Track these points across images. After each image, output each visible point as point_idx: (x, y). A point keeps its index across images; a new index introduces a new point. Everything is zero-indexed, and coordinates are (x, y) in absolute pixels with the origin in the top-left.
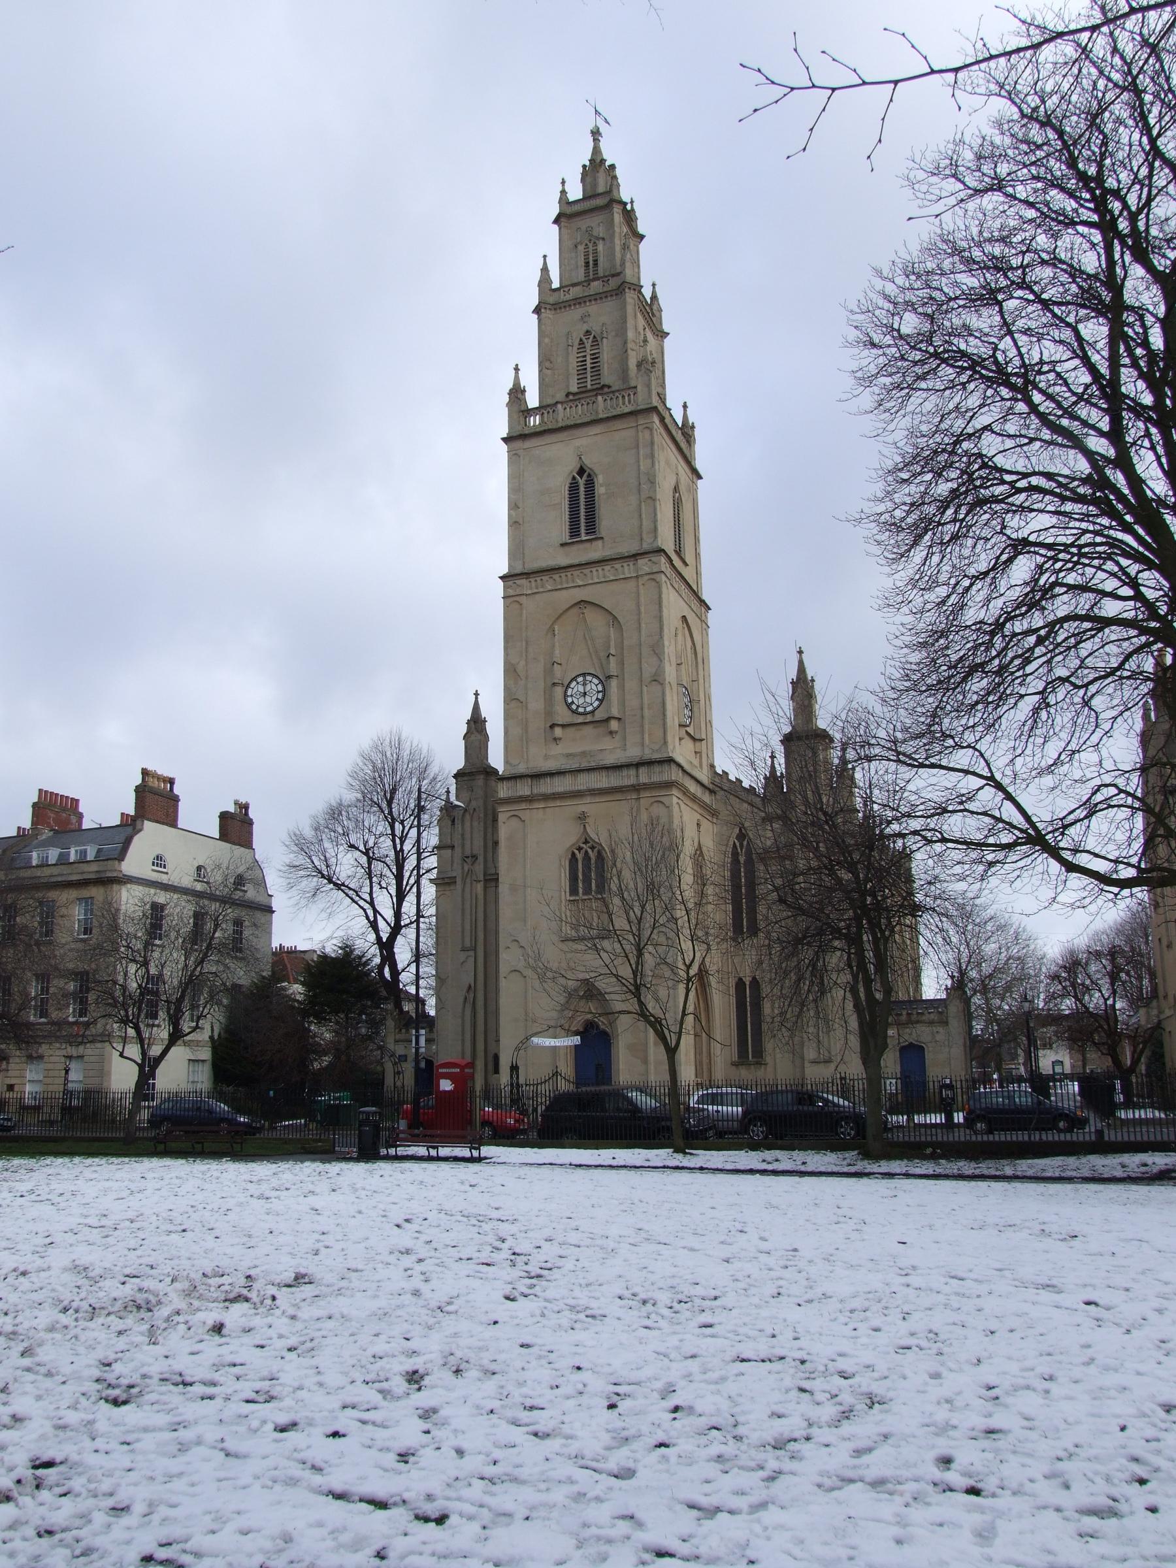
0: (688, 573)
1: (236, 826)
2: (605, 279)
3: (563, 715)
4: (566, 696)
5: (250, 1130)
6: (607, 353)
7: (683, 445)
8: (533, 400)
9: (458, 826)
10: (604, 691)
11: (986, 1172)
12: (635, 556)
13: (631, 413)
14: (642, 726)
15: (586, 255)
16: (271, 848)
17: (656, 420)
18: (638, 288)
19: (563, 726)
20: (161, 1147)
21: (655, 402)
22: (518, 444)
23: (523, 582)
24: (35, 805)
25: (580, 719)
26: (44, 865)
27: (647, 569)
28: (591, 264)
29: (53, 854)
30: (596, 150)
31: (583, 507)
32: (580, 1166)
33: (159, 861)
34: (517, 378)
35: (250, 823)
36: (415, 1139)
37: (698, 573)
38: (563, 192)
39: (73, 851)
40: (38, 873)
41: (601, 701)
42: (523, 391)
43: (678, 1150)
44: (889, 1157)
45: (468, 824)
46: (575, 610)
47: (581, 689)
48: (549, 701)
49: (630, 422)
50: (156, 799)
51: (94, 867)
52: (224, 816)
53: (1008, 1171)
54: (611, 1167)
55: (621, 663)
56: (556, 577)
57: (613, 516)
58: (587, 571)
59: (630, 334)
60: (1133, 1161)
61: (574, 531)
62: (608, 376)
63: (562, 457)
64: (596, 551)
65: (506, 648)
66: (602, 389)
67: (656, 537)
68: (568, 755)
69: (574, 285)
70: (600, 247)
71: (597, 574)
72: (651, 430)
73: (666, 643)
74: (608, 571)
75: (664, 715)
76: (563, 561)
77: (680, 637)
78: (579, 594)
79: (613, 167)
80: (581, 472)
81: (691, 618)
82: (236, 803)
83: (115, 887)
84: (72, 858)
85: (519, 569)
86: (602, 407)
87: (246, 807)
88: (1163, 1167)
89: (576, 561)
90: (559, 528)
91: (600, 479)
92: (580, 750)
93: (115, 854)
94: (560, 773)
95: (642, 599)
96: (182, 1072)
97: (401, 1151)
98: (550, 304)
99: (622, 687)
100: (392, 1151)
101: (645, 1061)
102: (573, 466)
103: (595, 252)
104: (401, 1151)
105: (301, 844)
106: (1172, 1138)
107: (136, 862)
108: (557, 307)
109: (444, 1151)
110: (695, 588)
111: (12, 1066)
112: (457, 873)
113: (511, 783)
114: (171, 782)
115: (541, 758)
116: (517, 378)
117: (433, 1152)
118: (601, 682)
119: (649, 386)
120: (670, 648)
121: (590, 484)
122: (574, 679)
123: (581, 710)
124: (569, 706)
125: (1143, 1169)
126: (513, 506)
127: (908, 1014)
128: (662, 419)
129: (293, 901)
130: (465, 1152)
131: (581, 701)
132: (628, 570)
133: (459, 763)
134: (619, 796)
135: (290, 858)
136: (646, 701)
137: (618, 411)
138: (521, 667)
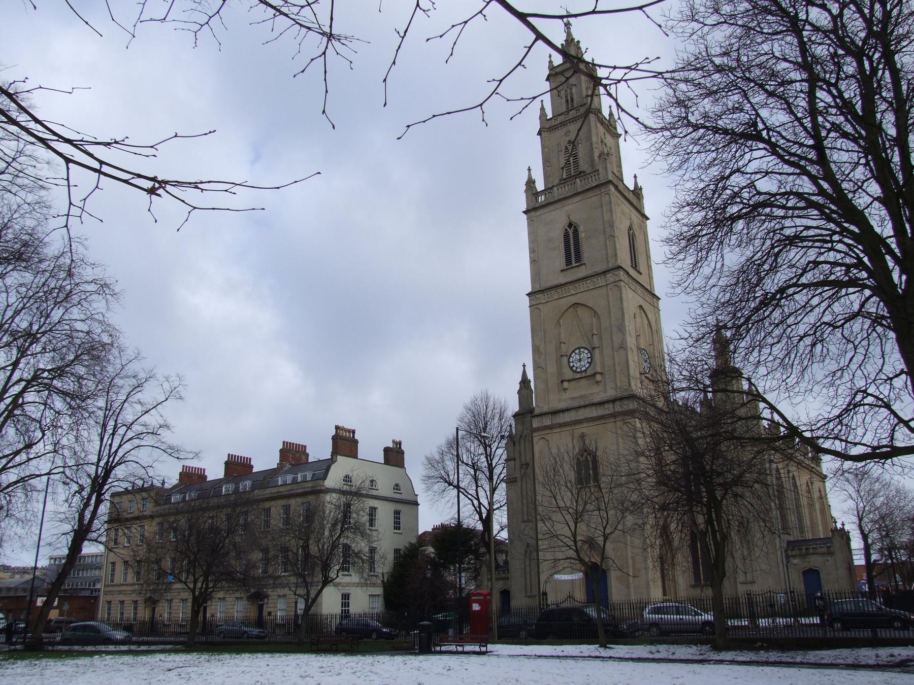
0: (642, 279)
1: (394, 455)
2: (577, 109)
3: (568, 374)
4: (569, 362)
5: (389, 636)
6: (582, 151)
7: (635, 201)
8: (540, 186)
9: (517, 444)
10: (591, 357)
11: (784, 660)
12: (604, 273)
13: (596, 186)
14: (615, 376)
15: (566, 96)
16: (415, 469)
17: (612, 188)
18: (599, 111)
19: (569, 381)
20: (315, 648)
21: (611, 177)
22: (533, 214)
23: (540, 296)
24: (281, 451)
25: (579, 376)
26: (285, 484)
27: (612, 280)
28: (569, 101)
29: (289, 478)
30: (569, 34)
31: (573, 249)
32: (540, 656)
33: (347, 479)
34: (530, 175)
35: (403, 453)
36: (472, 641)
37: (650, 277)
38: (551, 62)
39: (299, 476)
40: (281, 489)
41: (590, 363)
42: (534, 182)
43: (604, 646)
44: (728, 649)
45: (522, 445)
46: (571, 309)
47: (578, 357)
48: (560, 366)
49: (597, 191)
50: (344, 443)
51: (310, 485)
52: (386, 450)
53: (799, 659)
54: (558, 657)
55: (601, 339)
56: (559, 290)
57: (591, 250)
58: (577, 285)
59: (594, 139)
60: (884, 653)
61: (568, 261)
62: (584, 166)
63: (558, 218)
64: (582, 272)
65: (532, 337)
66: (581, 174)
67: (616, 260)
68: (572, 399)
69: (560, 115)
70: (574, 90)
71: (583, 286)
72: (609, 194)
73: (627, 324)
74: (589, 284)
75: (628, 368)
76: (562, 280)
77: (638, 318)
78: (573, 300)
79: (578, 42)
80: (570, 225)
81: (646, 306)
82: (393, 441)
83: (321, 495)
84: (299, 480)
85: (538, 288)
86: (579, 184)
87: (400, 443)
88: (904, 658)
89: (570, 280)
90: (560, 262)
91: (581, 229)
92: (578, 395)
93: (322, 476)
94: (568, 410)
95: (611, 299)
96: (365, 601)
97: (443, 648)
98: (547, 129)
99: (602, 353)
100: (438, 648)
101: (628, 587)
102: (562, 223)
103: (571, 93)
104: (443, 648)
105: (431, 462)
106: (912, 636)
107: (333, 479)
108: (551, 129)
109: (468, 648)
110: (648, 288)
111: (270, 601)
112: (518, 475)
113: (539, 419)
114: (354, 432)
115: (558, 401)
116: (530, 175)
117: (460, 649)
118: (589, 352)
119: (606, 168)
120: (630, 326)
121: (576, 232)
122: (573, 351)
123: (579, 370)
124: (571, 368)
125: (890, 659)
126: (532, 251)
127: (807, 549)
128: (616, 187)
129: (429, 498)
130: (477, 649)
131: (579, 364)
132: (601, 281)
133: (516, 408)
134: (603, 421)
135: (424, 473)
136: (616, 361)
137: (589, 186)
138: (542, 348)
